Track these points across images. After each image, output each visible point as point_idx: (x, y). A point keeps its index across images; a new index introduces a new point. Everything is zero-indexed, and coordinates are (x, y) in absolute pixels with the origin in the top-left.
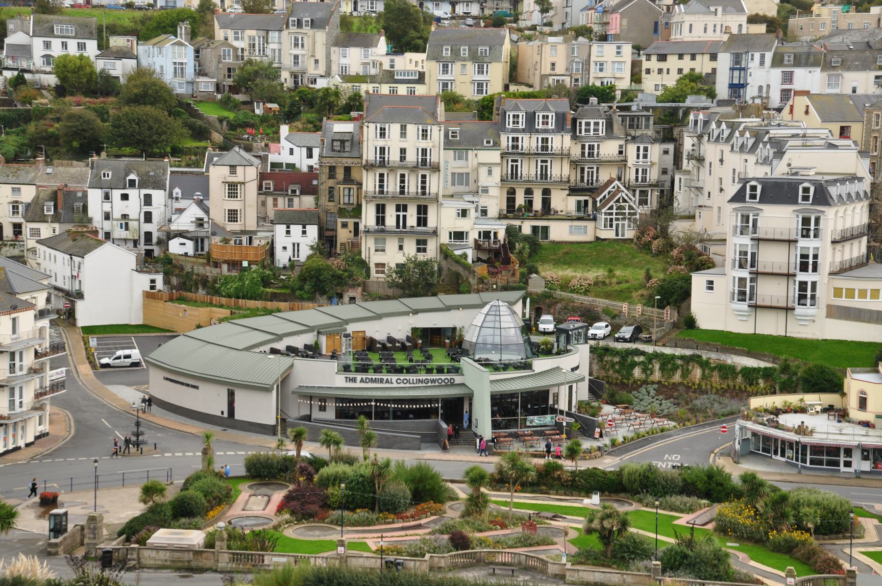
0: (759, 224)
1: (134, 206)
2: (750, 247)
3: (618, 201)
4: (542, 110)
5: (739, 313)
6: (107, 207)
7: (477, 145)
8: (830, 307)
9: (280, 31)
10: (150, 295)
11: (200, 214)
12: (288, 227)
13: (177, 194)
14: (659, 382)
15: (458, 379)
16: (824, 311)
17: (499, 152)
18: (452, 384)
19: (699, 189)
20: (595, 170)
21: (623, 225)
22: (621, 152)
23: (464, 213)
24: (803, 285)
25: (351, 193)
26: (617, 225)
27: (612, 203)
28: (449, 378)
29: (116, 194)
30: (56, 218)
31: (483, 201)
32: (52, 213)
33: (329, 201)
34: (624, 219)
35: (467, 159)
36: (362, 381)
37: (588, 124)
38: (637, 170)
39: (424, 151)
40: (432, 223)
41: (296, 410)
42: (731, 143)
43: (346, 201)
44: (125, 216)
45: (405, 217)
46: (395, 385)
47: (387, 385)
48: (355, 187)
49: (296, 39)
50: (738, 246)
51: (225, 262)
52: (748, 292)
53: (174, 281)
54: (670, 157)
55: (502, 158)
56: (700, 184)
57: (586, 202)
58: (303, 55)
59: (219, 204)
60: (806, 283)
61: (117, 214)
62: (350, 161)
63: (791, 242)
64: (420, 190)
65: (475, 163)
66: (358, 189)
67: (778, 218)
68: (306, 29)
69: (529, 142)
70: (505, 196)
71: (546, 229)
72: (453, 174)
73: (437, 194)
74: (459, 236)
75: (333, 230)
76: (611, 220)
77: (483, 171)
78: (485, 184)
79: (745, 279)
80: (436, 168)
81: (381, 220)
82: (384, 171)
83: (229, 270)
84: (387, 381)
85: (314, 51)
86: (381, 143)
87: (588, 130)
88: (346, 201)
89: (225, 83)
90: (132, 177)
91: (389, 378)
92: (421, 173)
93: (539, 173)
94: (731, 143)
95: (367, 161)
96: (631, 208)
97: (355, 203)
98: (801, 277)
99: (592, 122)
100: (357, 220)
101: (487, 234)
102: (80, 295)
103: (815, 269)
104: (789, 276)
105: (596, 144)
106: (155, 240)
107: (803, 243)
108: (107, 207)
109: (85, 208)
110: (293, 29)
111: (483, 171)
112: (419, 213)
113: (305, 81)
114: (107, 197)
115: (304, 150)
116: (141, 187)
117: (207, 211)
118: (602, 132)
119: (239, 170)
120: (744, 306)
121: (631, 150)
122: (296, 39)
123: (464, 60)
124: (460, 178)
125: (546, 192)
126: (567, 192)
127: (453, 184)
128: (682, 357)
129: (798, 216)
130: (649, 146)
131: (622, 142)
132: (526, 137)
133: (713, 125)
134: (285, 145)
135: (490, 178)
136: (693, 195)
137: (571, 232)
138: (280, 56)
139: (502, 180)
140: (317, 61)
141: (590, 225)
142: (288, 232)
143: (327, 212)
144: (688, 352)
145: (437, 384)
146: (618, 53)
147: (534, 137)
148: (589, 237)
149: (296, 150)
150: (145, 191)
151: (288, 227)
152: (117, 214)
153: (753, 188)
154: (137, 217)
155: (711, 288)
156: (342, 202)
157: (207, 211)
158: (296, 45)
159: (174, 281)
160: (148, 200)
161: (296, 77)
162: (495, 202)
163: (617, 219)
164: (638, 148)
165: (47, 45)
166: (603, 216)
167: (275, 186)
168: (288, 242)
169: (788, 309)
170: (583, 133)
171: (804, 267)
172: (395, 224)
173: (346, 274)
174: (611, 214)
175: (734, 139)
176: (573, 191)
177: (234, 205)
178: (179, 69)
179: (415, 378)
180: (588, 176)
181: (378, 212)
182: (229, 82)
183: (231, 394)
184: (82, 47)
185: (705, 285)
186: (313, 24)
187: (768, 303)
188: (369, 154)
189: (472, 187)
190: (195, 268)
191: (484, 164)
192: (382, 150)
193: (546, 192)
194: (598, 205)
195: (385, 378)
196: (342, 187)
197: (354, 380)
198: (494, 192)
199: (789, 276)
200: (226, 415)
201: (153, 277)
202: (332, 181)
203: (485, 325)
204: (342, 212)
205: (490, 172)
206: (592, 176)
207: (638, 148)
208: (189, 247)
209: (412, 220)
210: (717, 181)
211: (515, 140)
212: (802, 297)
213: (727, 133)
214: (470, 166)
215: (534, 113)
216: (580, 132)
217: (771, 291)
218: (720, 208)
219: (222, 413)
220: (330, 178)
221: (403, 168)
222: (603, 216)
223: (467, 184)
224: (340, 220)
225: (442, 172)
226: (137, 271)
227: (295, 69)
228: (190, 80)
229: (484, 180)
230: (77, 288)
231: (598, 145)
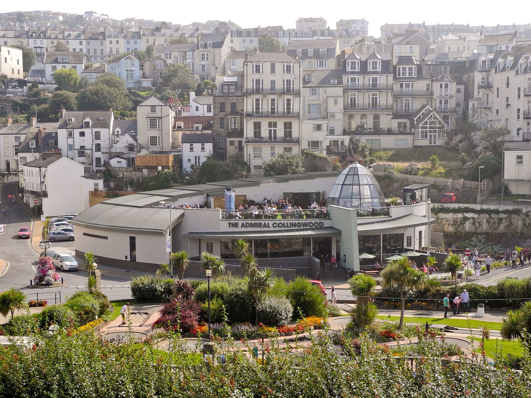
6: (70, 141)
7: (326, 84)
9: (194, 51)
10: (95, 194)
11: (131, 141)
12: (191, 145)
13: (118, 132)
14: (487, 233)
15: (326, 223)
18: (321, 227)
20: (410, 101)
21: (435, 136)
22: (428, 89)
23: (319, 128)
25: (237, 122)
26: (430, 136)
27: (426, 120)
28: (318, 221)
30: (36, 150)
31: (332, 123)
33: (221, 128)
34: (435, 132)
36: (243, 225)
37: (404, 69)
38: (441, 101)
39: (288, 82)
41: (186, 254)
42: (516, 69)
44: (82, 147)
45: (275, 131)
46: (272, 229)
48: (239, 117)
51: (145, 167)
53: (112, 184)
55: (344, 93)
56: (489, 106)
62: (235, 98)
64: (286, 110)
65: (325, 96)
66: (241, 118)
68: (209, 49)
72: (309, 105)
73: (299, 113)
74: (315, 144)
75: (224, 149)
76: (426, 132)
77: (331, 101)
78: (333, 111)
80: (298, 94)
81: (257, 126)
82: (259, 97)
84: (265, 226)
85: (214, 62)
86: (257, 76)
87: (404, 74)
88: (233, 127)
89: (158, 81)
91: (267, 222)
92: (287, 97)
93: (371, 103)
94: (516, 69)
95: (247, 89)
97: (239, 128)
99: (407, 67)
100: (240, 139)
101: (336, 142)
102: (45, 195)
106: (102, 162)
108: (70, 141)
109: (56, 142)
115: (206, 106)
116: (94, 126)
117: (136, 140)
121: (436, 86)
122: (203, 55)
123: (311, 58)
126: (392, 117)
128: (506, 212)
130: (449, 83)
131: (429, 82)
132: (361, 77)
139: (344, 109)
142: (192, 149)
143: (219, 135)
144: (510, 208)
145: (308, 227)
146: (411, 51)
147: (367, 77)
148: (410, 145)
150: (95, 130)
151: (191, 145)
152: (77, 146)
154: (91, 148)
156: (230, 128)
157: (136, 140)
158: (203, 59)
159: (112, 184)
160: (97, 136)
163: (430, 132)
170: (401, 76)
173: (232, 170)
174: (426, 128)
176: (396, 116)
179: (289, 222)
180: (406, 106)
181: (255, 128)
182: (160, 80)
183: (133, 241)
188: (249, 85)
190: (125, 174)
192: (258, 81)
195: (263, 223)
196: (229, 117)
197: (236, 225)
200: (129, 259)
202: (222, 113)
205: (336, 102)
206: (409, 106)
208: (124, 163)
211: (353, 80)
214: (321, 99)
216: (399, 75)
219: (126, 257)
220: (221, 111)
221: (273, 94)
225: (302, 97)
227: (203, 74)
228: (136, 81)
229: (332, 108)
230: (44, 190)
231: (412, 84)
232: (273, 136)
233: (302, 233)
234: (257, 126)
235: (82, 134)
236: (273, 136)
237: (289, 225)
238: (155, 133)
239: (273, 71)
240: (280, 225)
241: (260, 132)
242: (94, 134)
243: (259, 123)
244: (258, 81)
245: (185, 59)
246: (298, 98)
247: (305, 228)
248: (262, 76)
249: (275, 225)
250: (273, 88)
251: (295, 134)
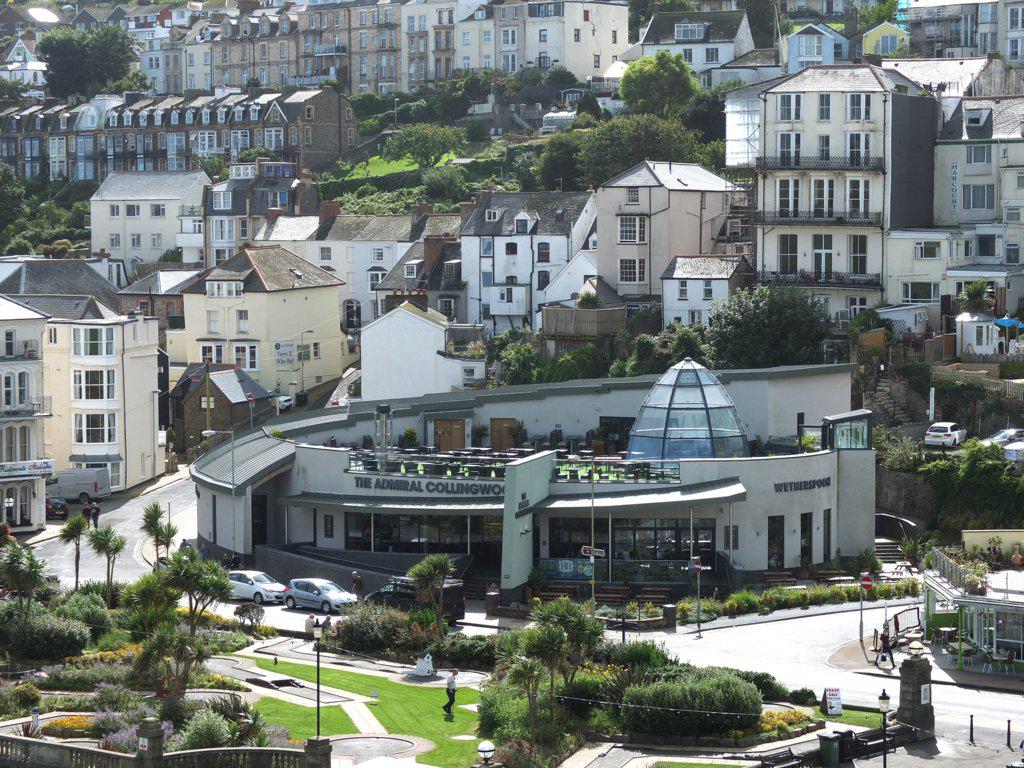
1: (523, 265)
6: (486, 265)
23: (930, 250)
29: (500, 243)
35: (989, 161)
45: (829, 257)
46: (425, 494)
47: (414, 494)
61: (500, 277)
72: (966, 188)
78: (1013, 204)
81: (788, 245)
82: (790, 176)
90: (522, 215)
92: (851, 176)
127: (966, 206)
145: (491, 495)
152: (500, 277)
154: (527, 281)
203: (674, 406)
232: (823, 270)
233: (473, 507)
234: (788, 245)
235: (512, 249)
236: (823, 270)
237: (455, 489)
238: (631, 252)
239: (825, 114)
240: (440, 488)
241: (795, 259)
242: (536, 248)
243: (794, 238)
244: (785, 139)
245: (977, 25)
246: (881, 177)
247: (486, 495)
248: (798, 126)
249: (431, 487)
250: (825, 154)
251: (873, 267)
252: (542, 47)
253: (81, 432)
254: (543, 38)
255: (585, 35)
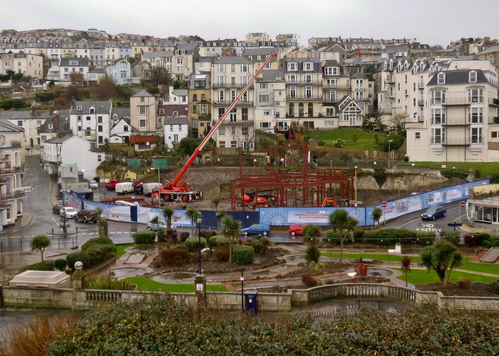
0: (446, 97)
1: (93, 124)
2: (441, 110)
3: (351, 105)
4: (306, 61)
5: (436, 151)
6: (79, 124)
8: (490, 144)
16: (486, 146)
17: (284, 84)
19: (393, 99)
21: (354, 119)
24: (475, 131)
29: (84, 117)
31: (278, 109)
32: (52, 128)
34: (354, 115)
35: (267, 88)
37: (330, 69)
38: (357, 93)
40: (250, 117)
43: (203, 112)
44: (89, 128)
45: (235, 115)
49: (178, 60)
50: (434, 110)
51: (137, 143)
52: (441, 137)
54: (372, 89)
56: (393, 96)
57: (332, 109)
58: (182, 67)
59: (136, 117)
60: (476, 129)
63: (466, 106)
65: (272, 90)
67: (457, 93)
68: (183, 55)
69: (301, 78)
70: (289, 107)
71: (312, 124)
72: (260, 96)
73: (253, 102)
74: (266, 125)
76: (348, 116)
77: (277, 93)
78: (278, 100)
79: (440, 129)
83: (139, 148)
85: (187, 65)
90: (92, 108)
96: (358, 109)
97: (208, 113)
98: (474, 126)
99: (333, 68)
100: (208, 122)
101: (281, 124)
103: (481, 121)
104: (466, 126)
105: (335, 80)
107: (473, 106)
110: (177, 55)
111: (277, 93)
112: (243, 113)
113: (183, 78)
114: (79, 118)
115: (181, 98)
118: (338, 73)
119: (146, 99)
120: (439, 146)
123: (259, 61)
124: (263, 98)
125: (310, 105)
127: (260, 101)
129: (469, 90)
131: (349, 79)
132: (299, 76)
133: (400, 63)
134: (171, 96)
135: (280, 97)
136: (388, 103)
137: (325, 124)
138: (171, 68)
140: (188, 69)
141: (336, 120)
142: (172, 129)
147: (303, 76)
149: (177, 98)
152: (85, 128)
153: (441, 76)
155: (419, 137)
158: (178, 62)
160: (100, 120)
161: (179, 77)
162: (283, 110)
163: (351, 115)
164: (357, 81)
165: (66, 70)
166: (343, 114)
167: (165, 111)
168: (172, 134)
169: (466, 146)
170: (328, 74)
171: (475, 120)
172: (230, 119)
174: (348, 112)
175: (414, 67)
176: (325, 104)
177: (144, 117)
178: (123, 74)
184: (81, 70)
185: (414, 135)
186: (186, 52)
187: (454, 143)
189: (271, 102)
191: (277, 90)
192: (222, 77)
193: (310, 105)
194: (339, 109)
196: (200, 105)
198: (283, 104)
199: (466, 126)
201: (99, 154)
204: (200, 118)
205: (280, 94)
207: (357, 81)
209: (239, 117)
210: (404, 92)
212: (474, 139)
213: (408, 65)
215: (302, 63)
216: (327, 73)
217: (456, 136)
218: (406, 106)
220: (194, 101)
221: (233, 88)
222: (343, 114)
223: (268, 101)
224: (199, 122)
226: (91, 151)
229: (277, 98)
235: (88, 118)
250: (233, 83)
252: (20, 67)
253: (333, 283)
254: (20, 64)
255: (32, 64)
